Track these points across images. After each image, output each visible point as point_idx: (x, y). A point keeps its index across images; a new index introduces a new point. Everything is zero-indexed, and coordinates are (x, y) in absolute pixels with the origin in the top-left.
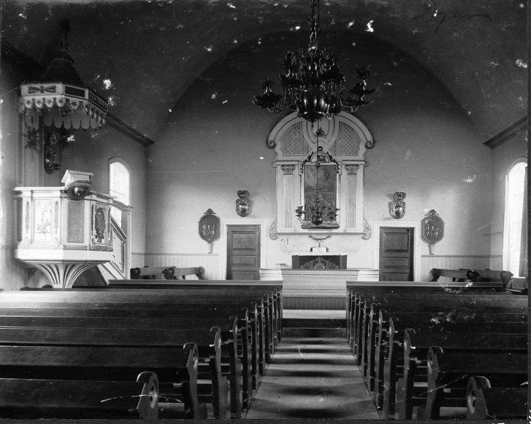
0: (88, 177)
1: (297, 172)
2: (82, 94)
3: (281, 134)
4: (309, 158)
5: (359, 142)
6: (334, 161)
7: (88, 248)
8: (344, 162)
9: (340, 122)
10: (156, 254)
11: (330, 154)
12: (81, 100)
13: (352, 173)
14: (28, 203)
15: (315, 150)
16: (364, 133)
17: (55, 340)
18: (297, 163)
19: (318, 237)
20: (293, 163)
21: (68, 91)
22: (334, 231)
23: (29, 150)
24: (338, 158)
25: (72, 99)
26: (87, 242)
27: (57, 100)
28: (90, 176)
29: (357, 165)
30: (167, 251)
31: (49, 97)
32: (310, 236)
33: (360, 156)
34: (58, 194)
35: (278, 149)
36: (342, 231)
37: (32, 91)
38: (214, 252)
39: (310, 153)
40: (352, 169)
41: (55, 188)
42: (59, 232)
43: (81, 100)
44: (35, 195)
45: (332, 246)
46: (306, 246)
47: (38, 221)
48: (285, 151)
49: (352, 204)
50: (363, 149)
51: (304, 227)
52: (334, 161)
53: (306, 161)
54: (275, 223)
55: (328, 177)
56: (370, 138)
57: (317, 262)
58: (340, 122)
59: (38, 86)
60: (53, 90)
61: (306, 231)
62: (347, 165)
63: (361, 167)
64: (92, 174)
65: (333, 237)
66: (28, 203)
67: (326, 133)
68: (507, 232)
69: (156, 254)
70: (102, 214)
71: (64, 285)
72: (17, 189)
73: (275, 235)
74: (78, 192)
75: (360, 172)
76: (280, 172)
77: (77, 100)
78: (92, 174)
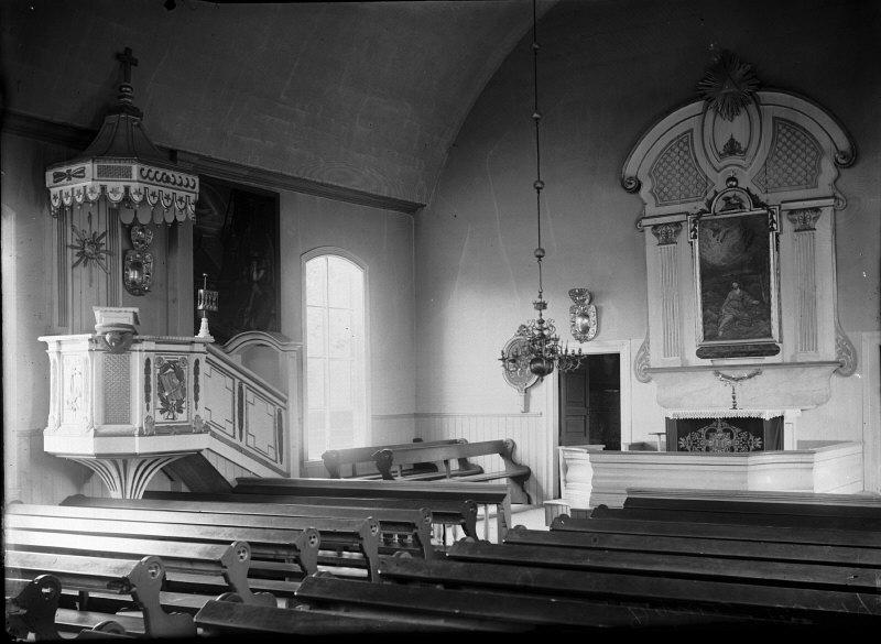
0: (131, 316)
1: (685, 235)
2: (128, 174)
3: (648, 164)
4: (709, 204)
5: (820, 152)
6: (763, 205)
7: (137, 432)
8: (784, 206)
9: (774, 118)
10: (434, 415)
11: (754, 191)
12: (127, 184)
13: (805, 228)
14: (54, 362)
15: (720, 185)
16: (830, 136)
17: (687, 470)
18: (683, 217)
19: (735, 374)
20: (676, 218)
21: (102, 173)
22: (768, 359)
23: (82, 271)
24: (771, 199)
25: (110, 185)
26: (137, 421)
27: (132, 191)
28: (135, 313)
29: (817, 209)
30: (447, 411)
31: (79, 185)
32: (716, 370)
33: (824, 186)
34: (86, 345)
35: (644, 192)
36: (788, 360)
37: (59, 177)
38: (533, 409)
39: (710, 195)
40: (805, 220)
41: (83, 336)
42: (113, 408)
43: (127, 184)
44: (64, 348)
45: (759, 397)
46: (710, 397)
47: (68, 395)
48: (661, 197)
49: (809, 301)
50: (828, 170)
51: (701, 354)
52: (763, 205)
53: (703, 212)
54: (645, 348)
55: (750, 244)
56: (844, 144)
57: (714, 431)
58: (774, 118)
59: (64, 170)
60: (81, 174)
61: (707, 362)
62: (792, 212)
63: (827, 215)
64: (136, 310)
65: (767, 372)
66: (54, 362)
67: (743, 146)
68: (643, 481)
69: (396, 417)
70: (180, 375)
71: (124, 492)
72: (41, 339)
73: (647, 372)
74: (111, 340)
75: (824, 227)
76: (649, 236)
77: (120, 186)
78: (136, 310)
